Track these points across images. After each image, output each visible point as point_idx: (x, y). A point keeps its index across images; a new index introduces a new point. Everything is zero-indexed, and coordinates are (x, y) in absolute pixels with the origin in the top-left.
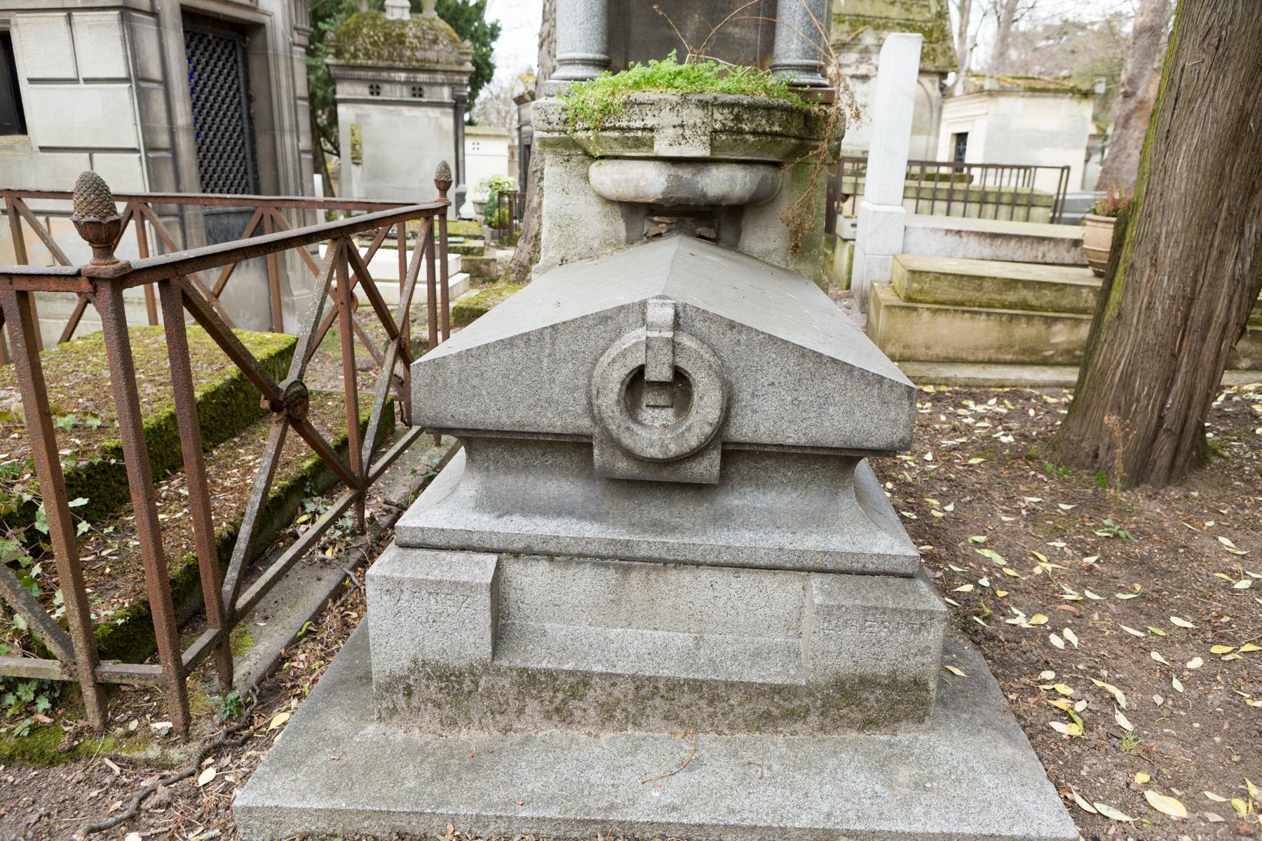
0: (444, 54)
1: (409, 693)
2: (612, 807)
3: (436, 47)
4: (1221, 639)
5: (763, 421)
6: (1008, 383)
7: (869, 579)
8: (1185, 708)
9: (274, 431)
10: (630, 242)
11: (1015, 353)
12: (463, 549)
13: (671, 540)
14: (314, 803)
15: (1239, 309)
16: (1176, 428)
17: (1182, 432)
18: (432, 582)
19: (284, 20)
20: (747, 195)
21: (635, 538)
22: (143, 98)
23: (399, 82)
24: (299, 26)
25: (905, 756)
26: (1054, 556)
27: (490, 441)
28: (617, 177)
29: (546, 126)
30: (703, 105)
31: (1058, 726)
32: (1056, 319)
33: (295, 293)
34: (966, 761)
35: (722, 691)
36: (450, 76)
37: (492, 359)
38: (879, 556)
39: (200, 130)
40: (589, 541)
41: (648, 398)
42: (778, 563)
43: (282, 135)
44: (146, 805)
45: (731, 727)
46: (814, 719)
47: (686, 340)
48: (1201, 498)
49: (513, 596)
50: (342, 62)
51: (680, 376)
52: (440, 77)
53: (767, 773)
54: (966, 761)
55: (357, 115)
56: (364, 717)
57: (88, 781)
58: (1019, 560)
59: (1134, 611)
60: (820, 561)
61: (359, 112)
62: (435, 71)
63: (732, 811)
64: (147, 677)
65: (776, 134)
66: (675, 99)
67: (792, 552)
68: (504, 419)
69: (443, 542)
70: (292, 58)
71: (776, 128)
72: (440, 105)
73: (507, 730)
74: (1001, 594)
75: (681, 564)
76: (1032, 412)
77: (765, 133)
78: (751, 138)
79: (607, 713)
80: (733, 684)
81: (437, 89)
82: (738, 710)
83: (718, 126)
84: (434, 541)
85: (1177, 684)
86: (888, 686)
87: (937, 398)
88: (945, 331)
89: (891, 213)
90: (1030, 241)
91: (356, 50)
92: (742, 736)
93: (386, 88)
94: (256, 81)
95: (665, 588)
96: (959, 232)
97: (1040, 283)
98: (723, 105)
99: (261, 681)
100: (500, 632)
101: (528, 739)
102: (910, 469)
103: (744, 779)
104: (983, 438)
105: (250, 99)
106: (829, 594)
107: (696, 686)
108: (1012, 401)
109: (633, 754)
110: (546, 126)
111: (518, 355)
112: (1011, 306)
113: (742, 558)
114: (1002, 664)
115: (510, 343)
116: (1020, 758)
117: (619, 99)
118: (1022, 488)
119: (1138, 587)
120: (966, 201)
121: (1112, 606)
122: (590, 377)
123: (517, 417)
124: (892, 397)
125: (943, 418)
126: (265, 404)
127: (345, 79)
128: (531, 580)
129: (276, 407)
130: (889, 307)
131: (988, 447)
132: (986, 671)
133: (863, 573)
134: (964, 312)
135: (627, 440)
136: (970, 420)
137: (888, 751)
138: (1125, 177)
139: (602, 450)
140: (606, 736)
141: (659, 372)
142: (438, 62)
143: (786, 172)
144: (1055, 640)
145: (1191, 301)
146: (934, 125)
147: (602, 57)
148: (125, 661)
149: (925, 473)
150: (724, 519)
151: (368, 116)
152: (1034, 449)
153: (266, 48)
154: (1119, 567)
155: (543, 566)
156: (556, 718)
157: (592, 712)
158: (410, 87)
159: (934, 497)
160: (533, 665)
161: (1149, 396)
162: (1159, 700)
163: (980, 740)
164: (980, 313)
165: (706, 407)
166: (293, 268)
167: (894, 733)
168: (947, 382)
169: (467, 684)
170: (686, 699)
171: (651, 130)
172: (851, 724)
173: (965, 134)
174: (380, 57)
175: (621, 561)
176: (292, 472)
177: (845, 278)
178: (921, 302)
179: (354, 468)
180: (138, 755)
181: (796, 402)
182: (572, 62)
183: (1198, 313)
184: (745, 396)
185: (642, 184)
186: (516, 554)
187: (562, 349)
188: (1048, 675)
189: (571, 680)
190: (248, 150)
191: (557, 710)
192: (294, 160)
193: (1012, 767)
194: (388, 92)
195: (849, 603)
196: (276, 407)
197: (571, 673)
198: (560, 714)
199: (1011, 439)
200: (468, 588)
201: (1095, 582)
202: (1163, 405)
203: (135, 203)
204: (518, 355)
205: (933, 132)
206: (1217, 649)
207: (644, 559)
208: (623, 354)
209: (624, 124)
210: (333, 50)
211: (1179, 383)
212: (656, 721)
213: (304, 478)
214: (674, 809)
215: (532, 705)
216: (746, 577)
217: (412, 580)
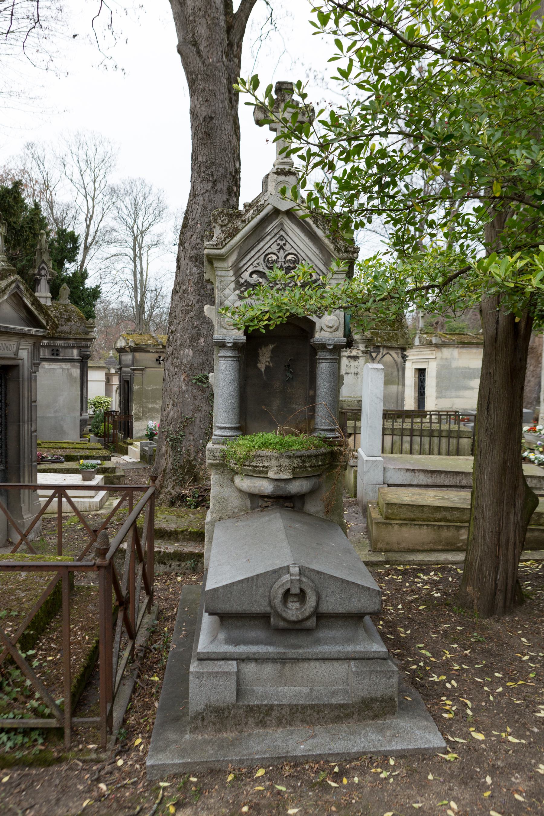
0: (75, 328)
1: (203, 719)
2: (288, 752)
3: (69, 324)
4: (512, 680)
5: (332, 604)
6: (440, 562)
7: (371, 661)
8: (492, 706)
10: (253, 508)
11: (443, 545)
12: (223, 659)
13: (300, 651)
14: (177, 761)
15: (519, 536)
17: (506, 590)
18: (215, 673)
19: (28, 361)
20: (308, 491)
21: (287, 651)
25: (389, 727)
26: (452, 651)
27: (230, 617)
28: (250, 485)
29: (213, 458)
30: (289, 457)
31: (445, 715)
32: (461, 527)
33: (25, 517)
34: (410, 727)
35: (322, 708)
36: (78, 342)
37: (235, 587)
38: (374, 652)
40: (271, 653)
41: (290, 599)
42: (339, 657)
43: (23, 425)
45: (326, 723)
46: (356, 716)
47: (304, 579)
48: (519, 620)
51: (302, 590)
52: (71, 343)
53: (341, 737)
54: (410, 727)
57: (71, 769)
58: (437, 654)
59: (481, 673)
60: (353, 655)
62: (69, 339)
63: (330, 749)
65: (320, 465)
66: (277, 455)
67: (343, 652)
68: (239, 609)
69: (216, 657)
71: (320, 463)
72: (71, 360)
74: (428, 668)
76: (450, 579)
77: (315, 466)
78: (309, 469)
80: (326, 705)
81: (69, 350)
82: (328, 715)
83: (295, 466)
84: (213, 657)
85: (491, 698)
86: (381, 701)
87: (404, 573)
88: (407, 535)
89: (376, 461)
90: (452, 474)
92: (331, 726)
95: (298, 670)
96: (413, 470)
97: (451, 508)
98: (297, 457)
100: (239, 693)
101: (250, 735)
102: (392, 613)
103: (333, 740)
104: (426, 595)
106: (357, 667)
107: (312, 707)
108: (441, 573)
109: (292, 735)
110: (213, 458)
111: (244, 585)
112: (439, 520)
113: (326, 656)
114: (427, 695)
116: (429, 724)
117: (252, 454)
118: (442, 620)
119: (484, 662)
120: (421, 436)
121: (473, 671)
122: (270, 592)
123: (244, 608)
125: (407, 584)
130: (377, 524)
131: (428, 599)
132: (420, 698)
133: (369, 659)
134: (415, 525)
135: (284, 615)
136: (420, 585)
137: (383, 726)
138: (529, 395)
139: (274, 618)
140: (280, 730)
141: (295, 590)
142: (70, 333)
143: (324, 478)
144: (448, 685)
145: (499, 534)
146: (401, 379)
149: (397, 615)
150: (318, 642)
152: (450, 599)
154: (479, 654)
156: (260, 725)
157: (274, 721)
158: (51, 349)
159: (402, 627)
160: (251, 703)
161: (489, 575)
162: (484, 704)
163: (415, 720)
164: (423, 525)
165: (311, 601)
166: (24, 501)
167: (385, 720)
168: (410, 563)
169: (226, 714)
170: (309, 712)
171: (267, 467)
172: (369, 718)
173: (424, 370)
177: (353, 489)
178: (393, 519)
180: (87, 758)
181: (341, 598)
183: (503, 538)
184: (324, 597)
185: (262, 488)
186: (243, 660)
188: (444, 698)
189: (266, 708)
191: (261, 721)
192: (28, 438)
193: (426, 728)
195: (364, 670)
197: (266, 705)
198: (262, 723)
199: (439, 594)
201: (467, 661)
202: (496, 578)
205: (400, 383)
206: (508, 684)
207: (290, 659)
208: (283, 585)
209: (254, 464)
211: (501, 569)
212: (298, 723)
214: (310, 750)
215: (251, 720)
216: (327, 663)
217: (207, 672)
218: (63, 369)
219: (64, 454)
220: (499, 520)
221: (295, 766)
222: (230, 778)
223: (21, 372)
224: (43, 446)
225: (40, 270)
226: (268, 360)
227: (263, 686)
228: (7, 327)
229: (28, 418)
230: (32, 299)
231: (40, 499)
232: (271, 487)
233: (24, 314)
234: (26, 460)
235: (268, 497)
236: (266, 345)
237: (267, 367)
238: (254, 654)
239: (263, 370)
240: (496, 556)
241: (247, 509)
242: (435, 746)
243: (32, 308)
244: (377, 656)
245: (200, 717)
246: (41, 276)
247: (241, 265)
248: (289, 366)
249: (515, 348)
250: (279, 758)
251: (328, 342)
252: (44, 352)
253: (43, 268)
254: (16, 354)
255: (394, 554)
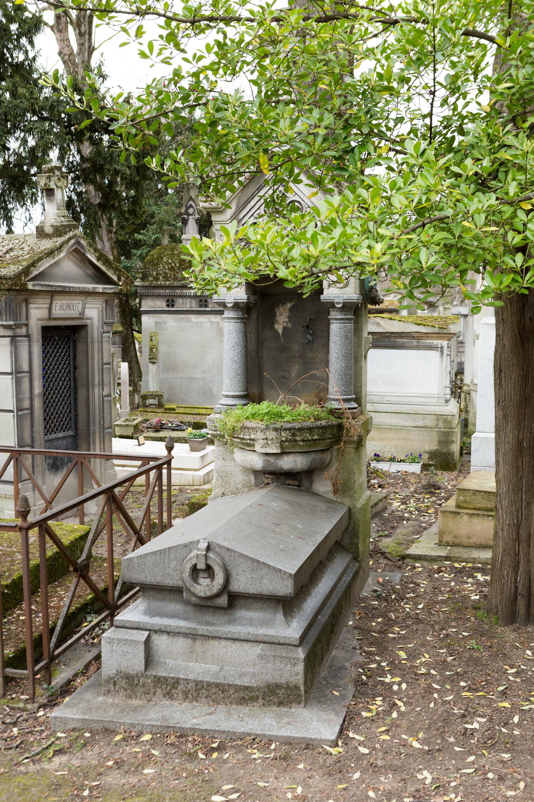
1: (115, 684)
7: (282, 646)
9: (75, 580)
12: (137, 629)
13: (210, 628)
14: (78, 717)
16: (524, 592)
20: (305, 468)
22: (18, 382)
23: (190, 297)
24: (108, 321)
30: (276, 430)
39: (45, 394)
41: (201, 575)
44: (20, 720)
45: (231, 703)
49: (155, 648)
50: (147, 283)
55: (156, 323)
56: (99, 695)
61: (157, 320)
64: (22, 674)
65: (316, 440)
66: (263, 427)
70: (102, 342)
71: (316, 437)
73: (149, 701)
75: (214, 638)
77: (308, 440)
78: (302, 443)
79: (186, 696)
82: (233, 696)
83: (283, 439)
88: (478, 528)
91: (158, 274)
93: (179, 301)
94: (80, 357)
98: (286, 429)
99: (62, 687)
100: (149, 659)
105: (75, 368)
107: (217, 685)
111: (157, 557)
113: (235, 636)
115: (155, 553)
117: (239, 425)
124: (285, 577)
126: (71, 569)
127: (148, 296)
128: (161, 642)
129: (76, 570)
134: (488, 516)
135: (192, 589)
140: (184, 704)
141: (201, 566)
145: (518, 527)
147: (242, 393)
148: (15, 668)
151: (165, 323)
153: (87, 338)
155: (165, 637)
157: (180, 695)
158: (198, 300)
160: (159, 674)
167: (290, 708)
168: (474, 560)
169: (136, 682)
170: (214, 690)
171: (253, 440)
172: (274, 703)
174: (176, 278)
175: (193, 636)
176: (82, 600)
178: (466, 508)
179: (110, 600)
180: (16, 706)
182: (228, 396)
184: (234, 575)
186: (156, 632)
187: (172, 556)
190: (72, 399)
191: (168, 693)
194: (180, 304)
195: (268, 654)
196: (76, 570)
197: (173, 678)
198: (169, 695)
200: (136, 642)
202: (516, 580)
203: (14, 454)
204: (157, 557)
210: (140, 276)
211: (521, 568)
212: (203, 699)
213: (87, 604)
215: (159, 691)
218: (212, 322)
219: (193, 421)
220: (518, 512)
221: (181, 736)
222: (118, 738)
223: (89, 332)
224: (177, 411)
225: (187, 209)
226: (286, 320)
227: (175, 660)
228: (65, 287)
229: (99, 382)
230: (97, 255)
231: (117, 468)
232: (261, 461)
233: (91, 271)
234: (97, 426)
235: (260, 471)
236: (284, 304)
237: (285, 328)
238: (166, 626)
239: (280, 331)
240: (515, 554)
241: (251, 486)
242: (323, 737)
243: (99, 264)
244: (287, 642)
245: (113, 681)
246: (188, 215)
247: (241, 216)
248: (307, 327)
249: (524, 305)
250: (168, 727)
251: (337, 300)
252: (191, 303)
253: (191, 206)
254: (83, 313)
255: (461, 550)
